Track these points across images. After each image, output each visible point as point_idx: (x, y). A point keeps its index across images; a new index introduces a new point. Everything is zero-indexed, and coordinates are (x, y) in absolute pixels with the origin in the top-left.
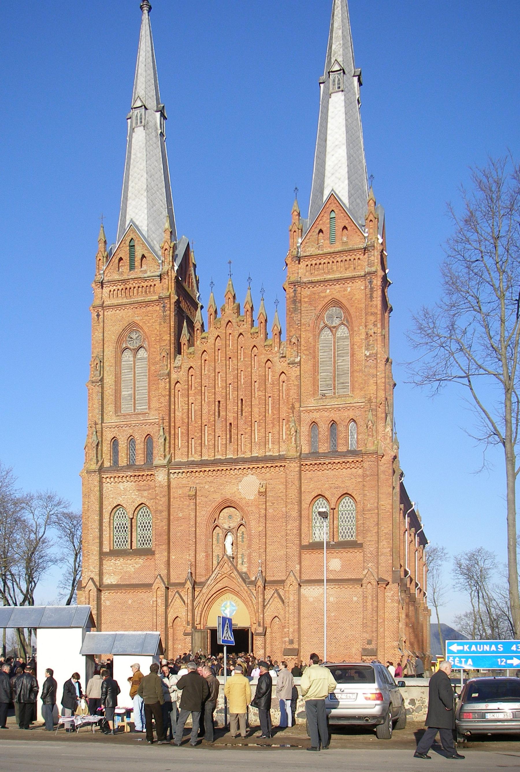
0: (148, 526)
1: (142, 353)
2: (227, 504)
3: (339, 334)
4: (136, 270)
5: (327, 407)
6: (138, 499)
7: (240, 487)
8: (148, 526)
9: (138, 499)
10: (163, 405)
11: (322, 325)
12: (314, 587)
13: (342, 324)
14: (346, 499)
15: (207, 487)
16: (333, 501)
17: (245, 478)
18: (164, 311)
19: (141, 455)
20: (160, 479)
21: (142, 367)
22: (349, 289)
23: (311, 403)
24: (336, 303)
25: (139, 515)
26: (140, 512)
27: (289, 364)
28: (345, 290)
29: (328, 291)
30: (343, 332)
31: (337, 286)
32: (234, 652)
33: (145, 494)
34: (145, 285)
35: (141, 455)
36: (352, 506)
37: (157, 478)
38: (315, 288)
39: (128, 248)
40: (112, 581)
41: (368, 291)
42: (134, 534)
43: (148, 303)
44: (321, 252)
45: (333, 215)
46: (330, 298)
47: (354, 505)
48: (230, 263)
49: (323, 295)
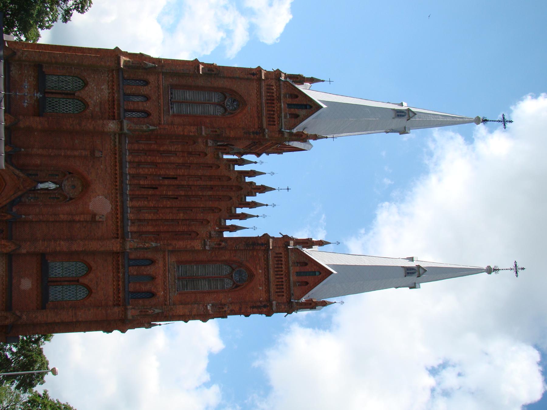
0: (67, 109)
1: (219, 111)
2: (86, 185)
3: (226, 280)
4: (287, 109)
5: (167, 273)
6: (92, 102)
7: (100, 197)
8: (67, 109)
9: (92, 102)
10: (176, 129)
11: (234, 266)
12: (4, 266)
13: (234, 283)
14: (83, 266)
15: (102, 167)
16: (85, 281)
17: (108, 202)
18: (253, 133)
19: (132, 106)
20: (110, 124)
21: (211, 110)
22: (261, 288)
23: (172, 260)
24: (251, 276)
25: (78, 101)
26: (80, 103)
27: (204, 240)
28: (260, 285)
29: (260, 271)
30: (228, 284)
31: (263, 279)
32: (543, 92)
33: (97, 109)
34: (276, 116)
35: (132, 106)
36: (80, 273)
37: (111, 122)
38: (263, 261)
39: (305, 103)
40: (14, 72)
41: (259, 304)
42: (60, 96)
43: (260, 118)
44: (290, 265)
45: (317, 273)
46: (255, 273)
47: (81, 298)
48: (288, 189)
49: (258, 267)
